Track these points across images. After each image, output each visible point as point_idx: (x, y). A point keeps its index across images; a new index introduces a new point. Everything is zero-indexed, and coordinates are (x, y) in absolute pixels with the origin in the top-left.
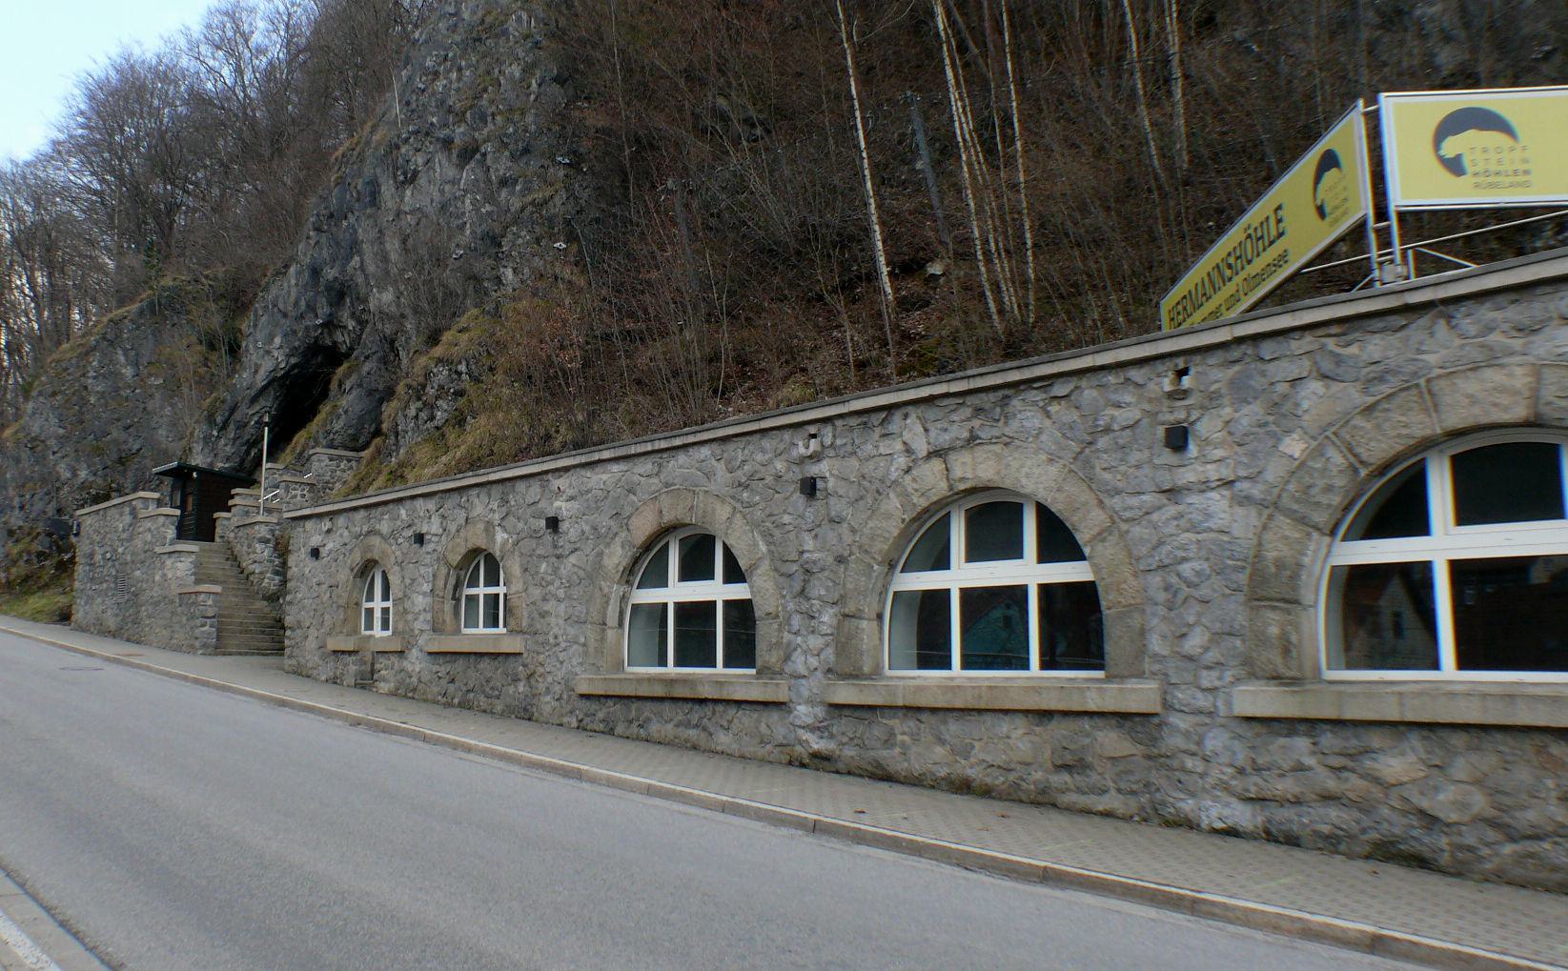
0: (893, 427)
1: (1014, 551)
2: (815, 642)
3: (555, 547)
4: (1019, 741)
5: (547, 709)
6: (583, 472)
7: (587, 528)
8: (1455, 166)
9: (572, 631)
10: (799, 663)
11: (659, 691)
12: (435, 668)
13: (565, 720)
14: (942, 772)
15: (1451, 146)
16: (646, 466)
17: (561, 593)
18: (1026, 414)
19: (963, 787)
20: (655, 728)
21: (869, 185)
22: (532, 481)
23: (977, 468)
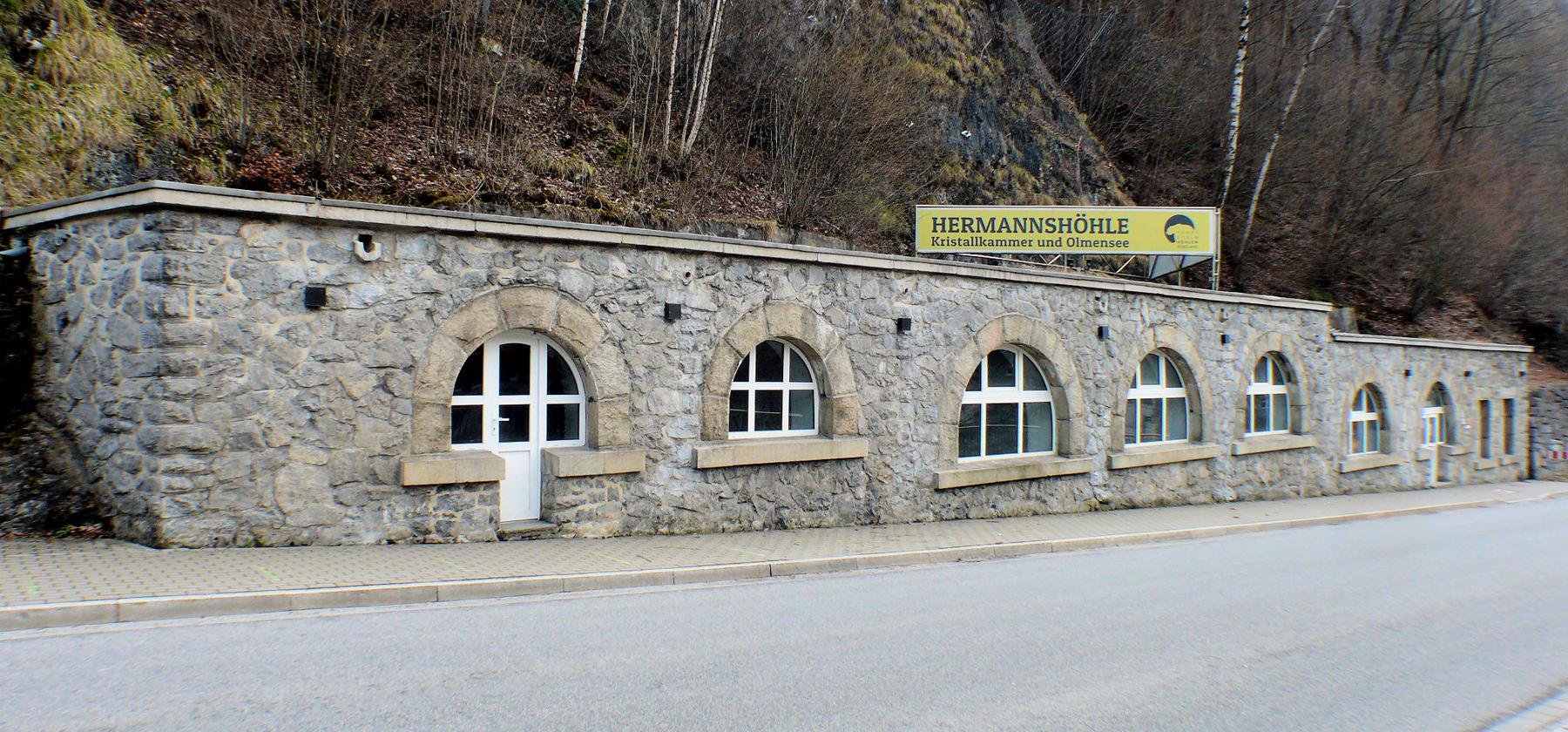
0: (1137, 305)
1: (1011, 382)
2: (1102, 431)
3: (899, 347)
4: (1178, 476)
5: (898, 510)
6: (932, 280)
7: (939, 336)
8: (1171, 238)
9: (923, 431)
10: (1093, 447)
11: (1016, 476)
12: (713, 487)
13: (921, 516)
14: (1154, 498)
15: (1171, 231)
16: (991, 290)
17: (908, 394)
18: (1183, 315)
19: (1161, 504)
20: (1003, 506)
21: (1265, 169)
22: (868, 275)
23: (1166, 337)
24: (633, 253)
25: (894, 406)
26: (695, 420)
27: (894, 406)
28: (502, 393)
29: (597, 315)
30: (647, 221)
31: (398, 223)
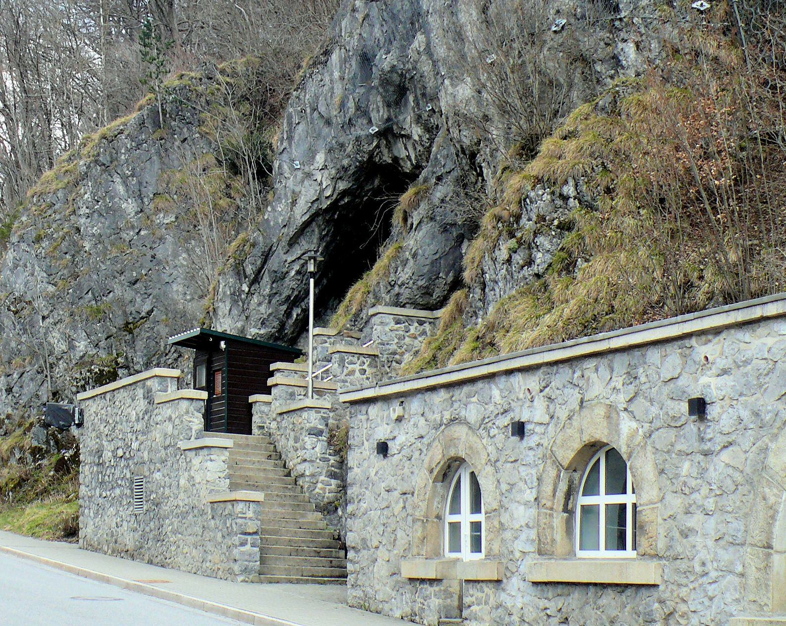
3: (702, 440)
17: (710, 504)
22: (669, 348)
24: (503, 379)
25: (695, 521)
26: (533, 534)
27: (695, 521)
28: (607, 505)
29: (484, 441)
30: (729, 298)
31: (416, 387)
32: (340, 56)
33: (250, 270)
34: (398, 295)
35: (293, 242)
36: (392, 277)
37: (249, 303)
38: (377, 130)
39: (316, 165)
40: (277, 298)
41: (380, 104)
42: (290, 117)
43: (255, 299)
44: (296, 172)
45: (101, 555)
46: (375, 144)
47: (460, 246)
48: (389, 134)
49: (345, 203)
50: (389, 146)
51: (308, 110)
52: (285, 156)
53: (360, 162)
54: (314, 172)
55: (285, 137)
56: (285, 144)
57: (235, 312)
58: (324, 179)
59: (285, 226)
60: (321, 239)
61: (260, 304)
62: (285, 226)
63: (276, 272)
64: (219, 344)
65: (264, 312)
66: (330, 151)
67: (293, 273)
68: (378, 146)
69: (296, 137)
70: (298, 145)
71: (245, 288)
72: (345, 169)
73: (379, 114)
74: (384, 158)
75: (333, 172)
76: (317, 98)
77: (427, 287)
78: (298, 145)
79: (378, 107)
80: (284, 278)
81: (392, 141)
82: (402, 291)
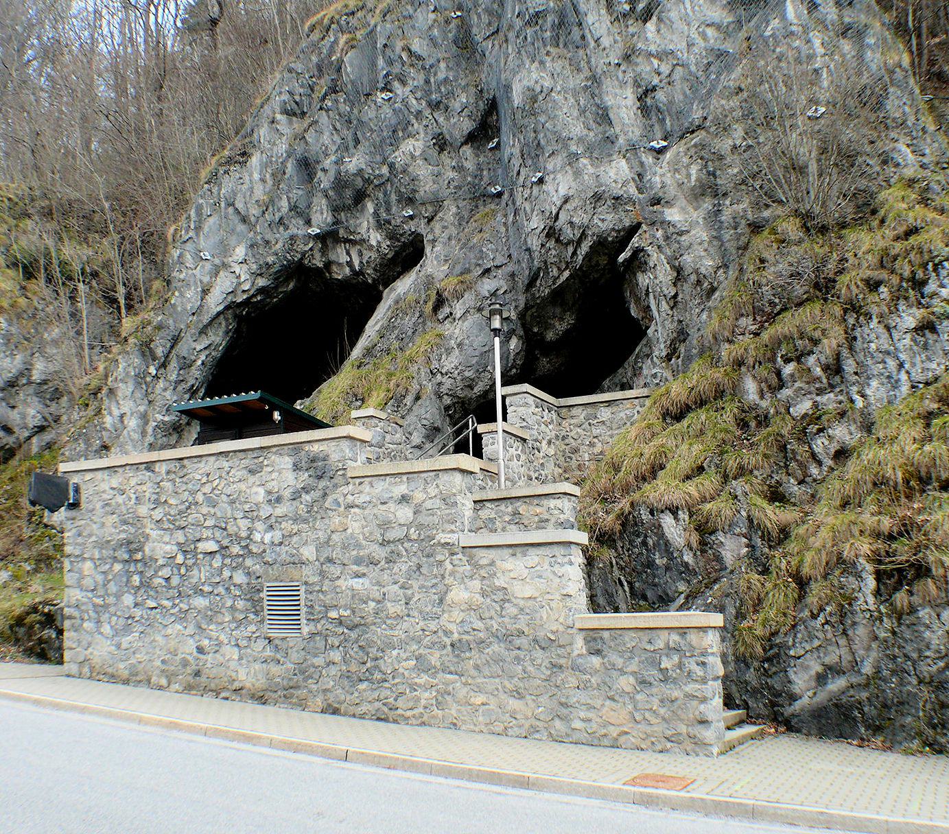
32: (261, 160)
33: (160, 352)
34: (440, 384)
35: (203, 331)
36: (435, 365)
37: (154, 387)
38: (319, 231)
39: (235, 258)
40: (183, 385)
41: (324, 207)
42: (199, 209)
43: (161, 384)
44: (204, 262)
45: (143, 690)
46: (310, 245)
47: (508, 341)
48: (328, 238)
49: (258, 301)
50: (324, 251)
51: (223, 205)
52: (189, 246)
53: (288, 261)
54: (232, 264)
55: (192, 226)
56: (191, 234)
57: (138, 395)
58: (243, 272)
59: (193, 314)
60: (227, 333)
61: (165, 390)
62: (193, 314)
63: (184, 358)
64: (272, 415)
65: (169, 398)
66: (252, 246)
67: (199, 362)
68: (311, 249)
69: (206, 229)
70: (207, 237)
71: (152, 370)
72: (268, 266)
73: (321, 218)
74: (314, 262)
75: (254, 267)
76: (235, 194)
77: (473, 380)
78: (207, 237)
79: (322, 209)
80: (191, 366)
81: (330, 245)
82: (444, 380)
